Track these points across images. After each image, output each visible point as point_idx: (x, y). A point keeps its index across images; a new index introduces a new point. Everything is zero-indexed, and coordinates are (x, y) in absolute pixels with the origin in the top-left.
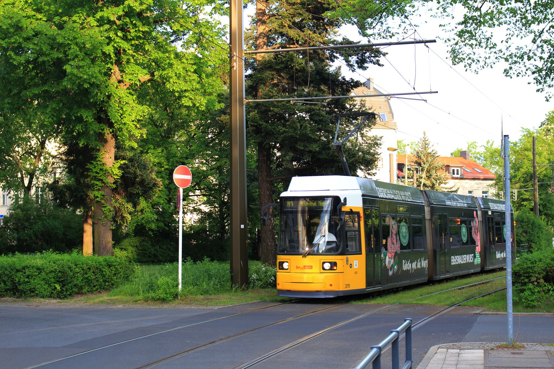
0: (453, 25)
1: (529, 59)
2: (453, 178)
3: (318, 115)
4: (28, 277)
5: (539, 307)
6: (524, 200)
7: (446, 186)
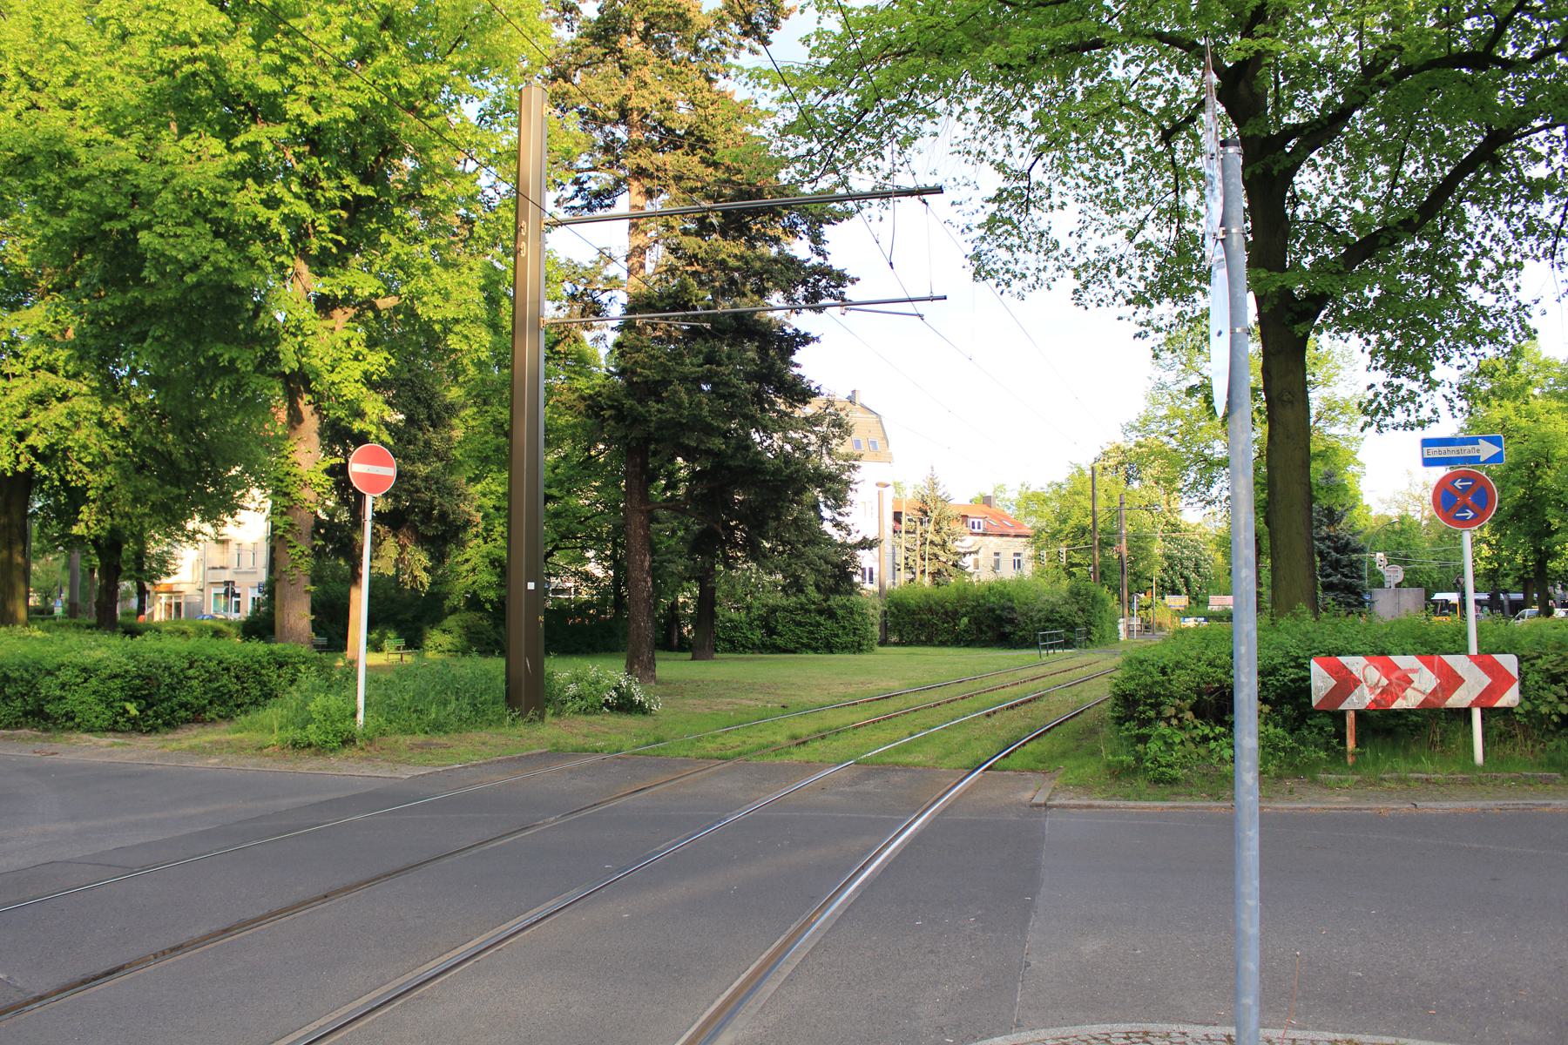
0: (977, 203)
1: (1120, 273)
2: (972, 534)
3: (727, 384)
4: (63, 686)
5: (1188, 783)
6: (1073, 565)
7: (963, 544)
